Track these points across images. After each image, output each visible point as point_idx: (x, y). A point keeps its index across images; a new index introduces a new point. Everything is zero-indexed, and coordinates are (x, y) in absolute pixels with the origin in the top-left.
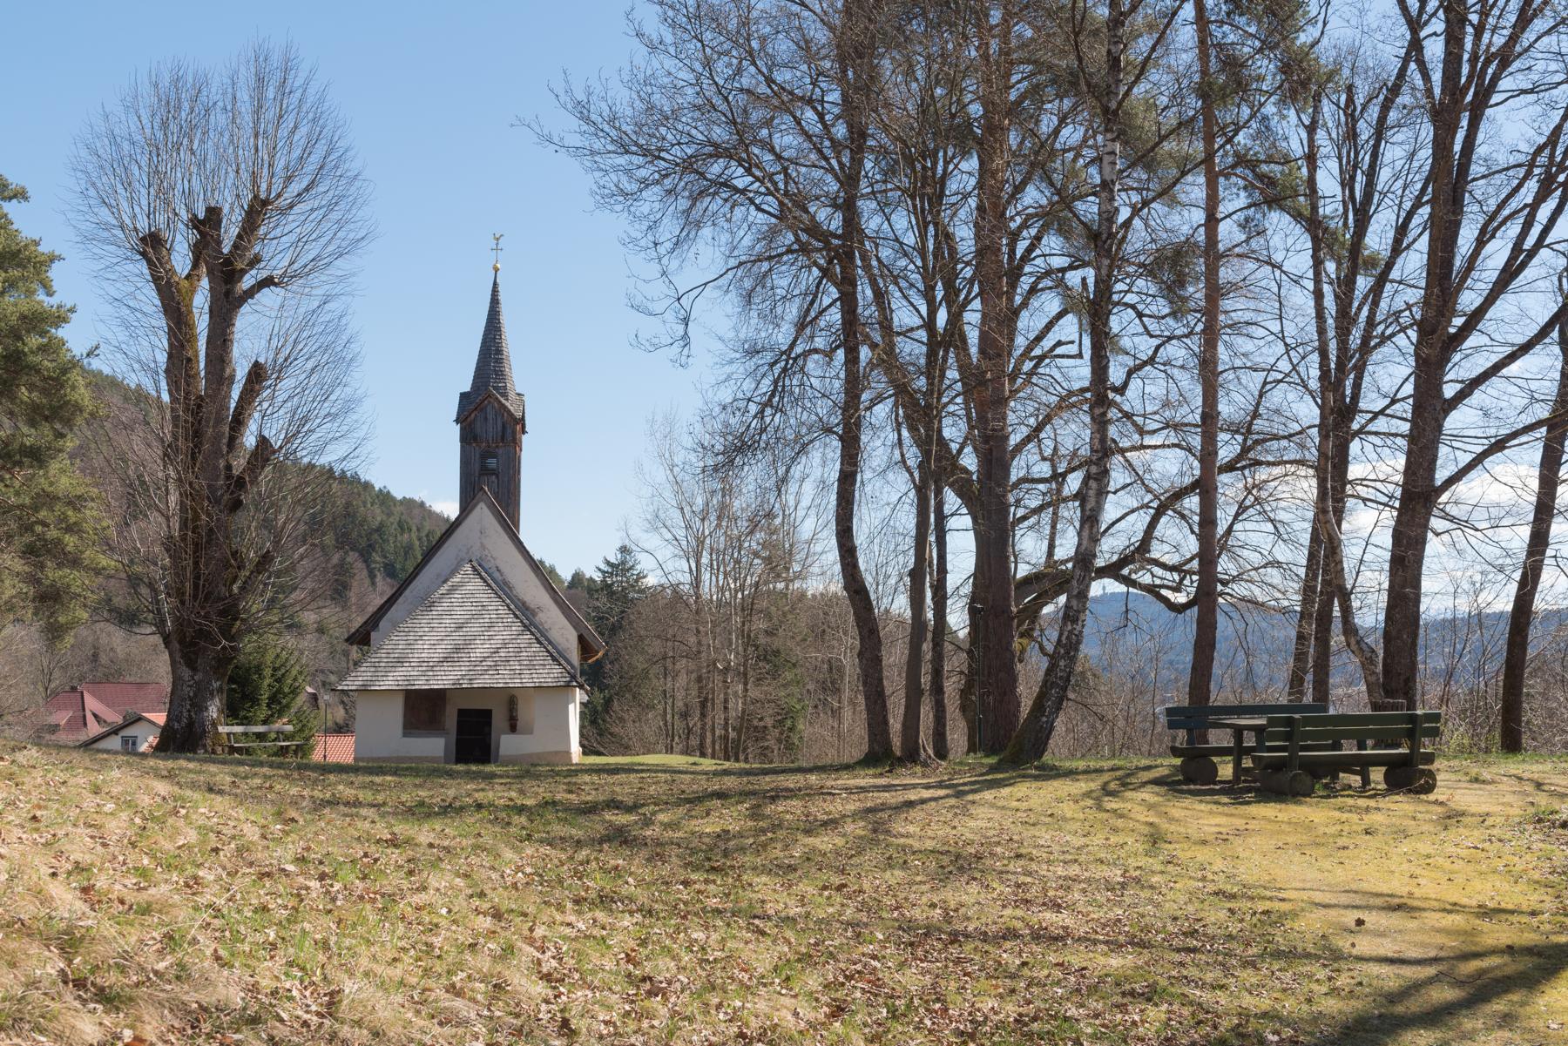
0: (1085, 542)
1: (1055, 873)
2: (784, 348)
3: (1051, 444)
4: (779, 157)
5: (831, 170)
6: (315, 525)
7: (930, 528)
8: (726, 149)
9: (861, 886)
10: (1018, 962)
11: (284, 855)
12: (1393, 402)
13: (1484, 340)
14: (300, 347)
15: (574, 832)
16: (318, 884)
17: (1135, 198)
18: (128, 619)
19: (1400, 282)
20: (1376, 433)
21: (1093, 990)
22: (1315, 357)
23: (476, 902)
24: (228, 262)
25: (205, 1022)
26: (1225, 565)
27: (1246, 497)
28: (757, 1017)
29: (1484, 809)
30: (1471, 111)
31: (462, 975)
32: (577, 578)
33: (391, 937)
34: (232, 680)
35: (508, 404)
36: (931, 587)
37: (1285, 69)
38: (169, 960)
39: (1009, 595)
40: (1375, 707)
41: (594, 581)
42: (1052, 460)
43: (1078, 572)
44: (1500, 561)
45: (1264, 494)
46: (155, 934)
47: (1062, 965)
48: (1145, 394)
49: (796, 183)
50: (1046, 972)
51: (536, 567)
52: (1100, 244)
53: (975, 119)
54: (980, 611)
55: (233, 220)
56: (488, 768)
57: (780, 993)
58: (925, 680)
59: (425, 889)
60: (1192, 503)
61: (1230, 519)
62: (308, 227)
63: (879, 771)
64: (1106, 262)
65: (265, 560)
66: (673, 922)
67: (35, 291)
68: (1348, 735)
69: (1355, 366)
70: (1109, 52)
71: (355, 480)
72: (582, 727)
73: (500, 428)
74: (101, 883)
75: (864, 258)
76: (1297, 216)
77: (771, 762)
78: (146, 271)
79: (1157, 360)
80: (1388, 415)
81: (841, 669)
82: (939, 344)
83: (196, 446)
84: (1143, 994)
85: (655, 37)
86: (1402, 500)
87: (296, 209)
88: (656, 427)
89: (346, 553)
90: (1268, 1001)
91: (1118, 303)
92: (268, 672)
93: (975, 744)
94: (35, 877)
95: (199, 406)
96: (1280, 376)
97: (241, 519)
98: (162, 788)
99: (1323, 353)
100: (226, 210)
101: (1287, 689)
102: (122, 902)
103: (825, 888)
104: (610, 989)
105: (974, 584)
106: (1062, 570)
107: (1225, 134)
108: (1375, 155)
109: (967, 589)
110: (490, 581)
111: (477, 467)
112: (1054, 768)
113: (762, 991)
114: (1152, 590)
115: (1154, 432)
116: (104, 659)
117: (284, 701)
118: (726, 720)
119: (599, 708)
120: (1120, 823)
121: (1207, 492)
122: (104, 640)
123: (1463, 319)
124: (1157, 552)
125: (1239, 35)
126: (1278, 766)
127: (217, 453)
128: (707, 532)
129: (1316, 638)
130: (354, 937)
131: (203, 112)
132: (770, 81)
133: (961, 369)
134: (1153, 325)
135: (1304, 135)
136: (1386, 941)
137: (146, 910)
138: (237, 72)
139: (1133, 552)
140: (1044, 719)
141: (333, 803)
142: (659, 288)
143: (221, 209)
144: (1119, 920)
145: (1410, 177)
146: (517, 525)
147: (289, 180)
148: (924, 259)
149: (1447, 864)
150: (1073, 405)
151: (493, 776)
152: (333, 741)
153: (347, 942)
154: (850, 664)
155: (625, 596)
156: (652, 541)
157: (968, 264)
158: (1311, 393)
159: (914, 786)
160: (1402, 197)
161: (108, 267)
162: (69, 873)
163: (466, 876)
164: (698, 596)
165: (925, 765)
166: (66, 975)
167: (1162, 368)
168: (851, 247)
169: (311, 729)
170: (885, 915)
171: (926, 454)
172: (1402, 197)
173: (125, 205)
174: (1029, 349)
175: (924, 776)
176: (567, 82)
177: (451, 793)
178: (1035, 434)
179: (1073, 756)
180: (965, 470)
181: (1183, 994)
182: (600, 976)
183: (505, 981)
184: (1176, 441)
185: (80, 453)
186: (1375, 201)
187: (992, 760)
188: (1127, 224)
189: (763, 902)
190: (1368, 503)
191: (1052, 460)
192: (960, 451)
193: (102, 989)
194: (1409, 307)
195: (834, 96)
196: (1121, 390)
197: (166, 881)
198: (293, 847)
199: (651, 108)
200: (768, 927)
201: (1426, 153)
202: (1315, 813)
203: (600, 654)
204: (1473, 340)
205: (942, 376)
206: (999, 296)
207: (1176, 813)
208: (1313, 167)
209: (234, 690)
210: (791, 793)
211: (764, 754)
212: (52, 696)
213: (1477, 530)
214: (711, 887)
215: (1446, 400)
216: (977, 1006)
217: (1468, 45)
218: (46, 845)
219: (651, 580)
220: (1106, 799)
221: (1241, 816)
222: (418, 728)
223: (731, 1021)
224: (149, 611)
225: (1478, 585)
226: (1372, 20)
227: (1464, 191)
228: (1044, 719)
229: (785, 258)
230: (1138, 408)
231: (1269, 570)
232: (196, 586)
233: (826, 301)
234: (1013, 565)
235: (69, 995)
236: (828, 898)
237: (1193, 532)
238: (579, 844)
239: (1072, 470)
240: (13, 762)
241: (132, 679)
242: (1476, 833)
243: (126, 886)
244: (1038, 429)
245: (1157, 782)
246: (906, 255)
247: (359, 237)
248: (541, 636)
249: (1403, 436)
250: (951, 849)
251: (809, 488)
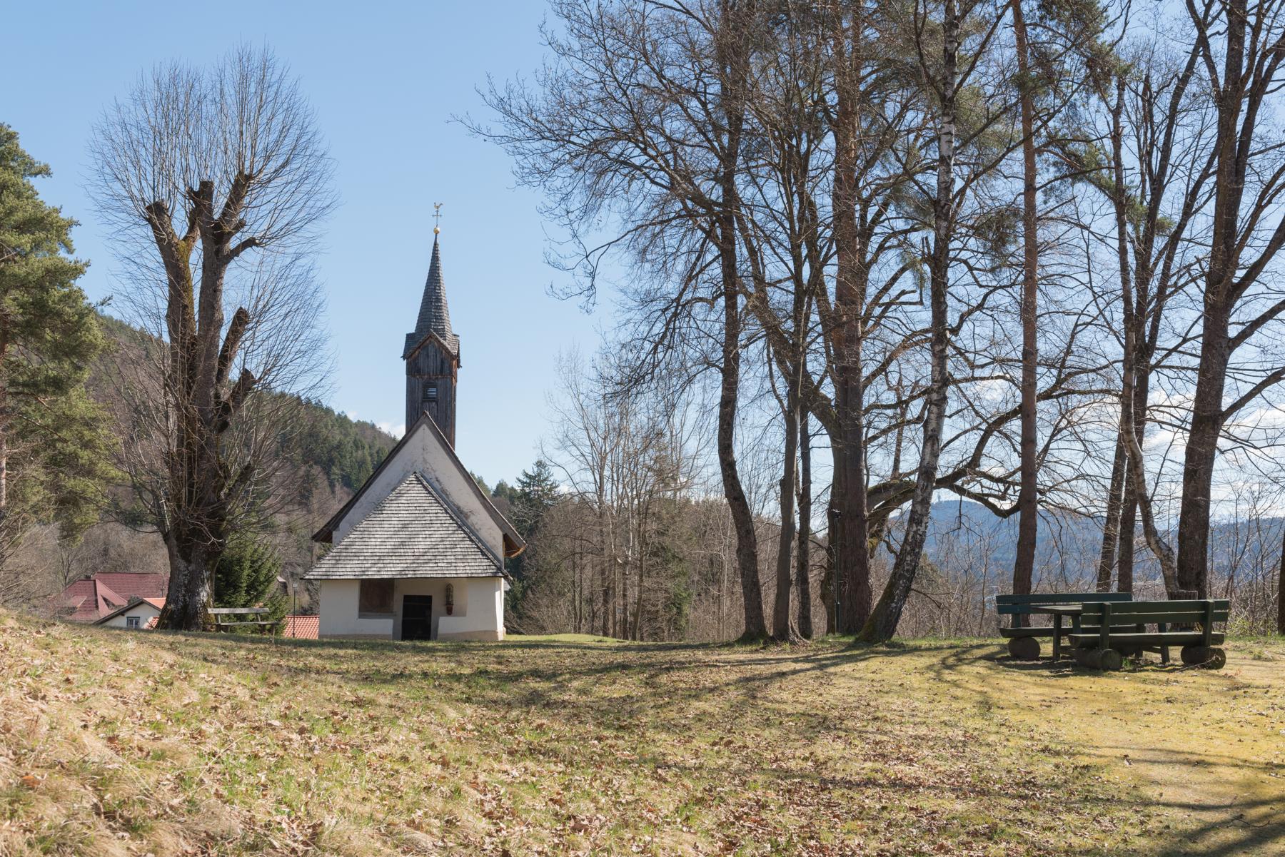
0: (927, 457)
1: (906, 732)
2: (674, 297)
3: (897, 376)
4: (669, 139)
5: (713, 149)
6: (285, 442)
7: (796, 442)
8: (625, 134)
9: (745, 742)
10: (878, 806)
11: (271, 711)
12: (1185, 340)
13: (1262, 289)
14: (276, 296)
15: (505, 696)
16: (299, 737)
17: (966, 170)
18: (133, 520)
19: (1190, 241)
20: (1170, 367)
21: (943, 829)
22: (1120, 304)
23: (429, 753)
24: (218, 226)
25: (212, 848)
26: (1043, 478)
27: (1060, 421)
28: (664, 849)
29: (1266, 682)
30: (1250, 96)
31: (420, 813)
32: (501, 488)
33: (360, 781)
34: (218, 571)
35: (446, 343)
36: (798, 494)
37: (1090, 64)
38: (182, 797)
39: (862, 502)
40: (1171, 596)
41: (515, 490)
42: (898, 389)
43: (922, 482)
44: (1275, 475)
45: (1075, 419)
46: (169, 776)
47: (916, 809)
48: (974, 335)
49: (683, 160)
50: (902, 815)
51: (468, 477)
52: (939, 209)
53: (832, 107)
54: (837, 515)
55: (222, 191)
56: (430, 644)
57: (681, 830)
58: (793, 573)
59: (386, 741)
60: (1015, 425)
61: (1047, 439)
62: (284, 198)
63: (754, 648)
64: (945, 224)
65: (247, 471)
66: (590, 771)
67: (57, 250)
68: (1151, 620)
69: (1153, 310)
70: (946, 50)
71: (318, 406)
72: (505, 611)
73: (439, 363)
74: (123, 733)
75: (740, 220)
76: (1101, 187)
77: (663, 640)
78: (151, 234)
79: (986, 306)
80: (1180, 352)
81: (721, 564)
82: (805, 292)
83: (190, 377)
84: (984, 834)
85: (564, 43)
86: (1194, 424)
87: (273, 183)
88: (562, 363)
89: (311, 466)
90: (1090, 841)
91: (955, 259)
92: (247, 564)
93: (833, 626)
94: (70, 729)
95: (193, 344)
96: (1089, 319)
97: (226, 438)
98: (169, 657)
99: (1127, 300)
100: (216, 184)
101: (1096, 581)
102: (141, 749)
103: (714, 744)
104: (541, 825)
105: (833, 494)
106: (906, 482)
107: (1040, 118)
108: (1169, 135)
109: (827, 497)
110: (431, 489)
111: (420, 395)
112: (901, 646)
113: (667, 828)
114: (981, 498)
115: (983, 366)
116: (112, 553)
117: (260, 588)
118: (625, 606)
119: (519, 596)
120: (959, 692)
121: (1028, 416)
122: (113, 538)
123: (1244, 272)
124: (986, 465)
125: (1046, 36)
126: (1092, 645)
127: (208, 383)
128: (608, 450)
129: (1121, 539)
130: (329, 781)
131: (196, 103)
132: (661, 76)
133: (820, 313)
134: (982, 279)
135: (1110, 118)
136: (1187, 792)
137: (161, 756)
138: (223, 71)
139: (966, 466)
140: (894, 605)
141: (307, 670)
142: (572, 247)
143: (212, 183)
144: (962, 772)
145: (1198, 152)
146: (453, 443)
147: (268, 158)
148: (791, 222)
149: (1237, 728)
150: (916, 344)
151: (433, 650)
152: (300, 621)
153: (325, 784)
154: (729, 559)
155: (541, 502)
156: (563, 457)
157: (827, 226)
158: (1115, 333)
159: (785, 660)
160: (1191, 169)
161: (119, 231)
162: (97, 726)
163: (419, 732)
164: (601, 502)
165: (793, 643)
166: (99, 808)
167: (990, 313)
168: (731, 212)
169: (282, 611)
170: (765, 766)
171: (793, 385)
172: (1191, 169)
173: (134, 180)
174: (878, 297)
175: (792, 652)
176: (491, 84)
177: (401, 664)
178: (883, 369)
179: (915, 637)
180: (825, 398)
181: (1018, 834)
182: (532, 814)
183: (456, 818)
184: (1001, 374)
185: (95, 382)
186: (1168, 173)
187: (850, 640)
188: (962, 192)
189: (664, 755)
190: (1164, 426)
191: (898, 389)
192: (821, 382)
193: (129, 820)
194: (1199, 261)
195: (715, 89)
196: (955, 331)
197: (175, 733)
198: (278, 705)
199: (562, 103)
200: (668, 775)
201: (1212, 133)
202: (1120, 685)
203: (521, 550)
204: (1253, 289)
205: (807, 318)
206: (854, 253)
207: (1005, 684)
208: (1117, 147)
209: (219, 579)
210: (682, 666)
211: (655, 634)
212: (70, 584)
213: (1256, 448)
214: (621, 742)
215: (1230, 339)
216: (846, 842)
217: (1247, 44)
218: (77, 702)
219: (564, 489)
220: (947, 671)
221: (1061, 687)
223: (642, 853)
224: (151, 513)
225: (1256, 494)
226: (1165, 21)
227: (1245, 164)
228: (894, 605)
229: (674, 223)
230: (970, 347)
231: (1080, 481)
232: (190, 492)
233: (709, 258)
234: (865, 477)
235: (101, 823)
236: (718, 752)
237: (1015, 450)
238: (509, 705)
239: (912, 398)
240: (48, 635)
241: (136, 570)
242: (1260, 702)
243: (143, 737)
244: (888, 362)
245: (988, 658)
246: (775, 218)
247: (324, 205)
248: (472, 534)
249: (1193, 369)
250: (818, 712)
251: (693, 414)
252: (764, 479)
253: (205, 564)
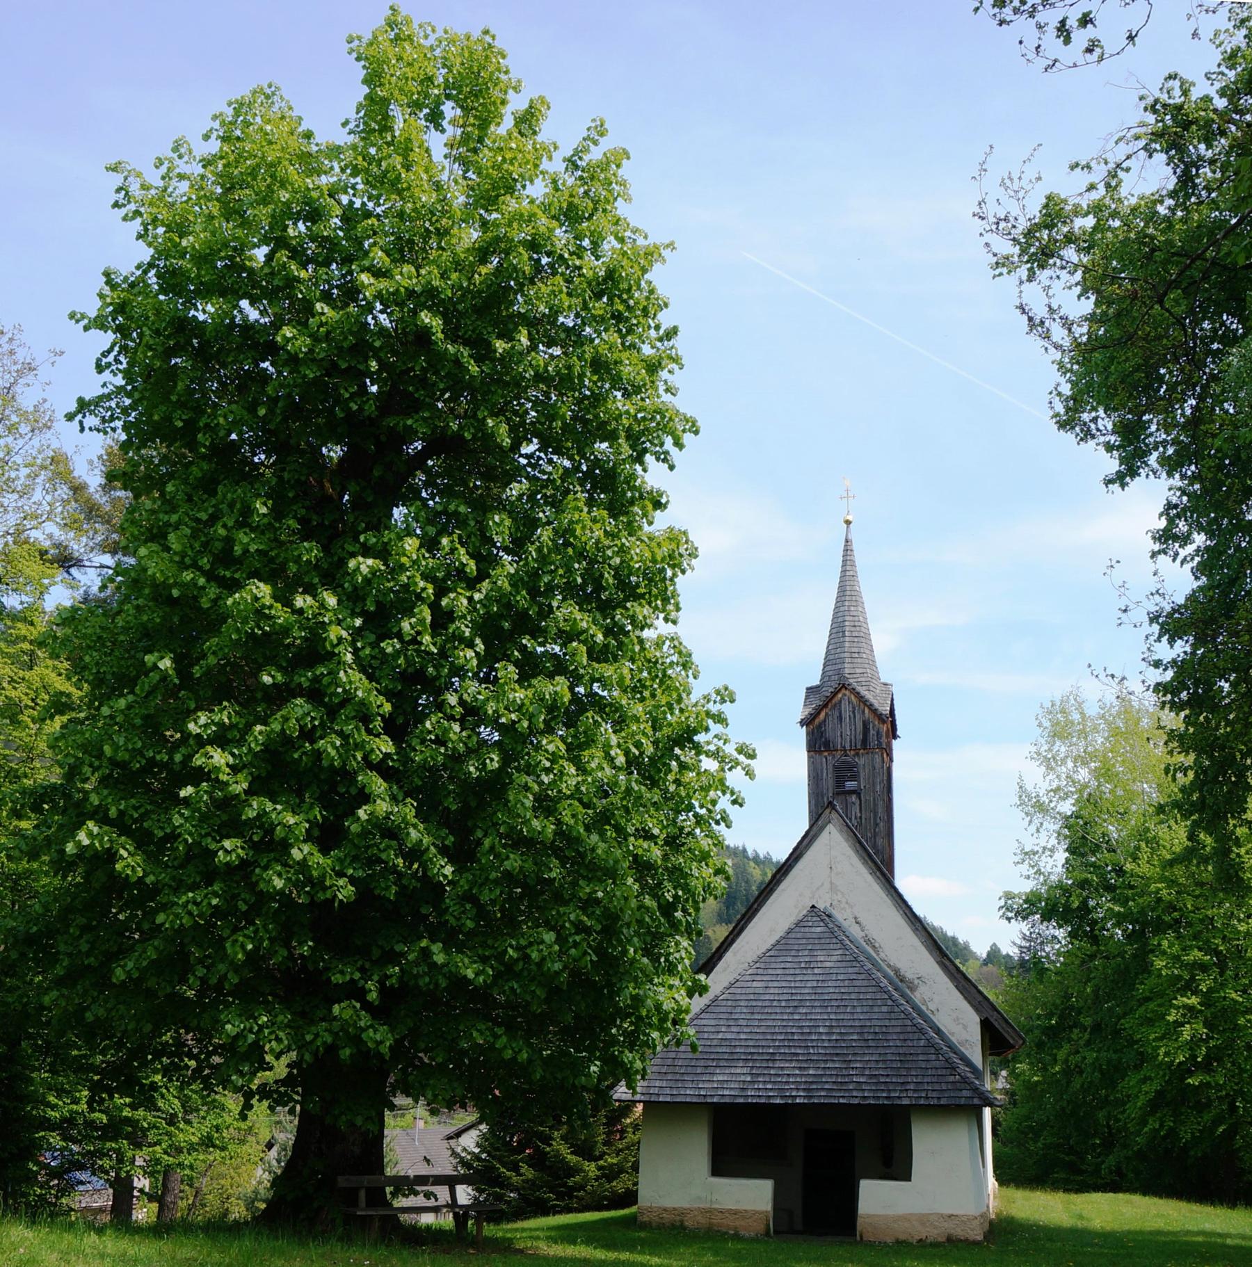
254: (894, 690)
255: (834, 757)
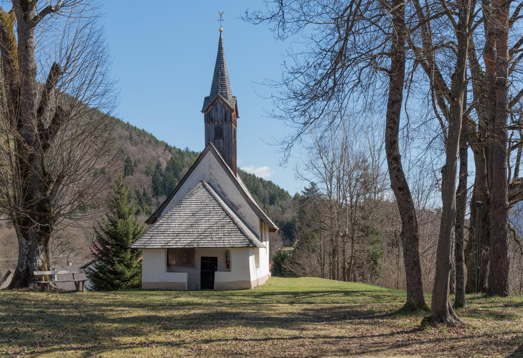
32: (297, 196)
35: (228, 102)
54: (479, 205)
222: (182, 266)
252: (428, 182)
253: (39, 241)
254: (237, 99)
255: (214, 124)
